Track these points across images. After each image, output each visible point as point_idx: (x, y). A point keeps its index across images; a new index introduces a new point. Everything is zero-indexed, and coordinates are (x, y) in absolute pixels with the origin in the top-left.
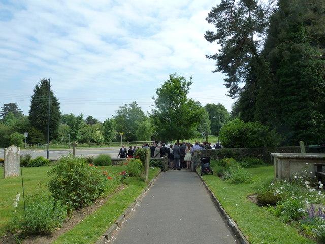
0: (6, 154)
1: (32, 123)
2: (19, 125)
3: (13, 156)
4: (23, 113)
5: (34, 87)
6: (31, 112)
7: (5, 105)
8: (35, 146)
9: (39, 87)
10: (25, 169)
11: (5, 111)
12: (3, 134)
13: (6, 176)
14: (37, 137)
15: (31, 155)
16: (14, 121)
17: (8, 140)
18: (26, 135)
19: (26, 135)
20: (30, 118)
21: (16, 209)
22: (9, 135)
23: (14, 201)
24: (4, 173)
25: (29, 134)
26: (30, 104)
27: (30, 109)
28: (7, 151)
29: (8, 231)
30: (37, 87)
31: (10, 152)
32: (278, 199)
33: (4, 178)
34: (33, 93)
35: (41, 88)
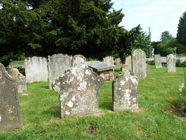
0: (168, 59)
1: (178, 41)
2: (171, 43)
3: (172, 60)
4: (172, 36)
5: (179, 19)
6: (177, 34)
7: (162, 33)
8: (181, 55)
9: (182, 18)
10: (178, 68)
11: (162, 36)
12: (163, 49)
13: (168, 71)
14: (182, 49)
15: (180, 60)
16: (168, 41)
17: (165, 52)
18: (175, 49)
19: (175, 49)
20: (177, 38)
21: (181, 92)
22: (166, 49)
23: (180, 87)
24: (167, 69)
25: (177, 48)
26: (177, 29)
27: (177, 32)
28: (168, 57)
29: (176, 105)
30: (181, 18)
31: (170, 57)
32: (18, 68)
33: (167, 72)
34: (178, 22)
35: (183, 18)
